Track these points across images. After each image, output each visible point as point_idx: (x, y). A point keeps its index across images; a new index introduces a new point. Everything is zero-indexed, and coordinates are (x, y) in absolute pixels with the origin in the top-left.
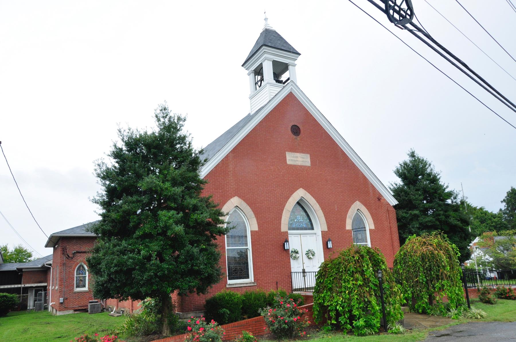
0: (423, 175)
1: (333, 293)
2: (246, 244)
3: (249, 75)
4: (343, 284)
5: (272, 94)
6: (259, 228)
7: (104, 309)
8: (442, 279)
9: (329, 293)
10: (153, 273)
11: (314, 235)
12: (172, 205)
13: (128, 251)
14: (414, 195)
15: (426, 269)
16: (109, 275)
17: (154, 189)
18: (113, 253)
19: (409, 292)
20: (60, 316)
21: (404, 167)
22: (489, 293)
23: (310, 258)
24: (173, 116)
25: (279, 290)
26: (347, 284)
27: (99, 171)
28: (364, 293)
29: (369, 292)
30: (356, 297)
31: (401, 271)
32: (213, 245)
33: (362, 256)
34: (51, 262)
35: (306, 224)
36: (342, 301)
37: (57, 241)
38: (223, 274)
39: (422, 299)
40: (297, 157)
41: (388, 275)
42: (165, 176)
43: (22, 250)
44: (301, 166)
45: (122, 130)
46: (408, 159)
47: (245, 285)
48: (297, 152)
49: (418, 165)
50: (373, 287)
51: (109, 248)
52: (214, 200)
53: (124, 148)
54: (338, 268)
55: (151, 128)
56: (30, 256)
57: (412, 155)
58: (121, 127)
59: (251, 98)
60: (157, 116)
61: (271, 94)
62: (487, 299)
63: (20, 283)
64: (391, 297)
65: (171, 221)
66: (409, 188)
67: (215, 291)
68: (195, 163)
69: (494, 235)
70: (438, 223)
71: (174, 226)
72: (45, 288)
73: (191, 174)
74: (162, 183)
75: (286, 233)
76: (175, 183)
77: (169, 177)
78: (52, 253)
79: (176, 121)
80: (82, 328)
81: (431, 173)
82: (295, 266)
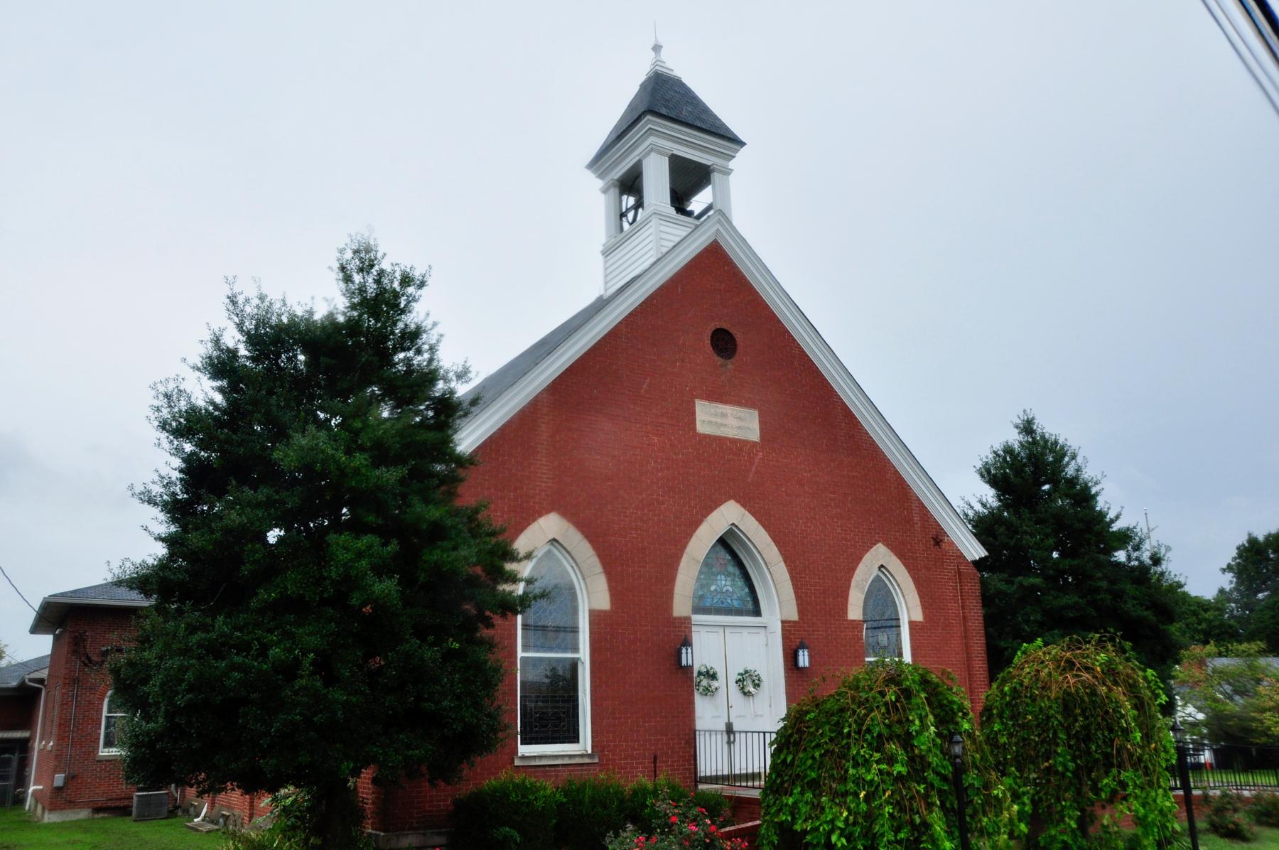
1: (820, 795)
3: (605, 191)
4: (851, 771)
7: (177, 808)
8: (1119, 766)
9: (809, 796)
11: (762, 631)
12: (371, 518)
13: (234, 646)
14: (1032, 535)
15: (1076, 736)
16: (169, 716)
18: (185, 652)
19: (1026, 799)
20: (51, 827)
21: (1005, 458)
22: (1235, 810)
23: (746, 694)
24: (389, 270)
25: (662, 779)
27: (165, 413)
28: (912, 798)
29: (926, 796)
30: (888, 809)
31: (1003, 740)
32: (482, 642)
33: (907, 693)
34: (44, 674)
35: (740, 599)
36: (847, 819)
38: (506, 727)
39: (1062, 820)
40: (724, 415)
41: (979, 749)
42: (356, 433)
45: (241, 299)
46: (1014, 438)
48: (726, 402)
49: (1043, 454)
50: (937, 782)
51: (174, 636)
52: (494, 517)
53: (243, 351)
54: (838, 723)
55: (322, 298)
57: (1028, 427)
58: (237, 290)
59: (607, 252)
60: (343, 269)
61: (662, 244)
62: (1231, 826)
64: (985, 814)
65: (364, 563)
66: (1017, 513)
67: (481, 777)
68: (449, 410)
69: (1209, 655)
71: (370, 578)
74: (346, 454)
75: (685, 623)
77: (364, 439)
79: (396, 285)
81: (1077, 478)
82: (707, 715)
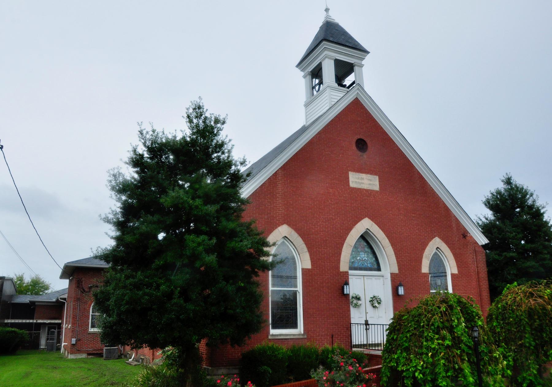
0: (522, 206)
1: (410, 354)
2: (296, 286)
4: (425, 343)
5: (333, 100)
6: (312, 265)
7: (122, 355)
9: (405, 354)
10: (174, 315)
11: (381, 278)
12: (203, 228)
16: (119, 315)
17: (180, 206)
18: (125, 287)
20: (72, 360)
23: (374, 307)
25: (336, 346)
26: (430, 343)
27: (113, 183)
29: (460, 356)
30: (443, 361)
31: (498, 330)
32: (254, 283)
33: (451, 307)
34: (66, 296)
35: (371, 263)
36: (423, 365)
37: (73, 272)
39: (529, 369)
43: (39, 281)
44: (367, 191)
45: (144, 132)
47: (292, 337)
50: (466, 349)
51: (120, 280)
52: (258, 226)
53: (146, 155)
54: (418, 321)
56: (47, 288)
57: (508, 181)
59: (307, 105)
60: (188, 117)
61: (332, 99)
63: (33, 319)
64: (490, 365)
66: (503, 222)
67: (255, 343)
70: (542, 269)
71: (204, 255)
72: (59, 326)
73: (230, 191)
75: (346, 274)
76: (208, 199)
77: (200, 193)
78: (67, 287)
79: (212, 123)
80: (91, 378)
81: (533, 205)
82: (356, 316)
